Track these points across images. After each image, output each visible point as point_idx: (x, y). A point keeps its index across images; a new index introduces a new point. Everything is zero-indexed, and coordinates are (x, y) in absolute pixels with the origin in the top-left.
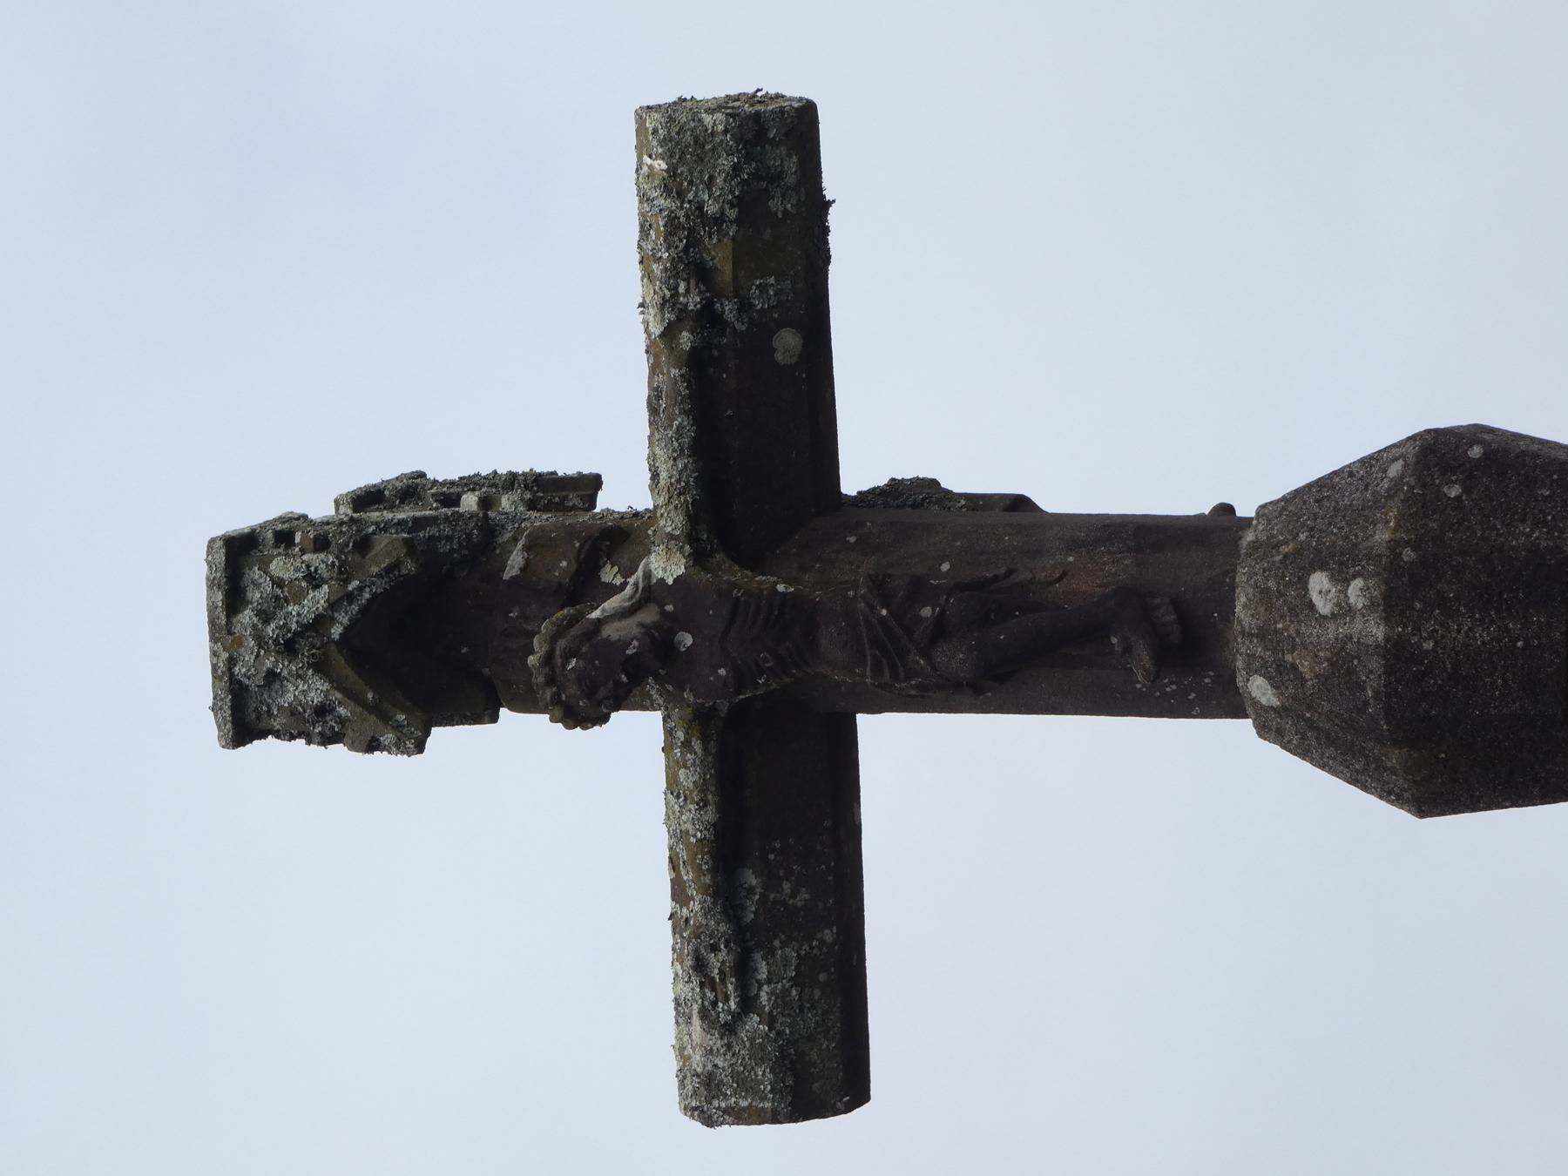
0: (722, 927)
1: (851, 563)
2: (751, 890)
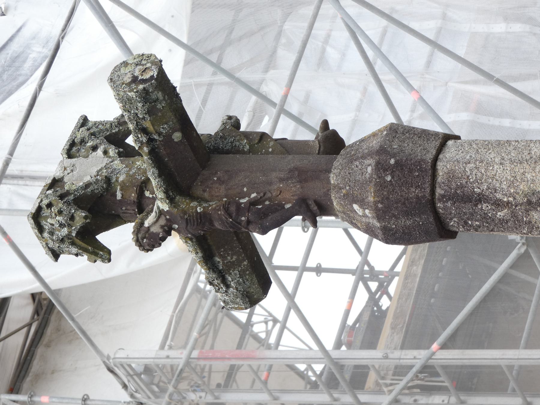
0: (214, 276)
1: (217, 188)
2: (219, 262)
